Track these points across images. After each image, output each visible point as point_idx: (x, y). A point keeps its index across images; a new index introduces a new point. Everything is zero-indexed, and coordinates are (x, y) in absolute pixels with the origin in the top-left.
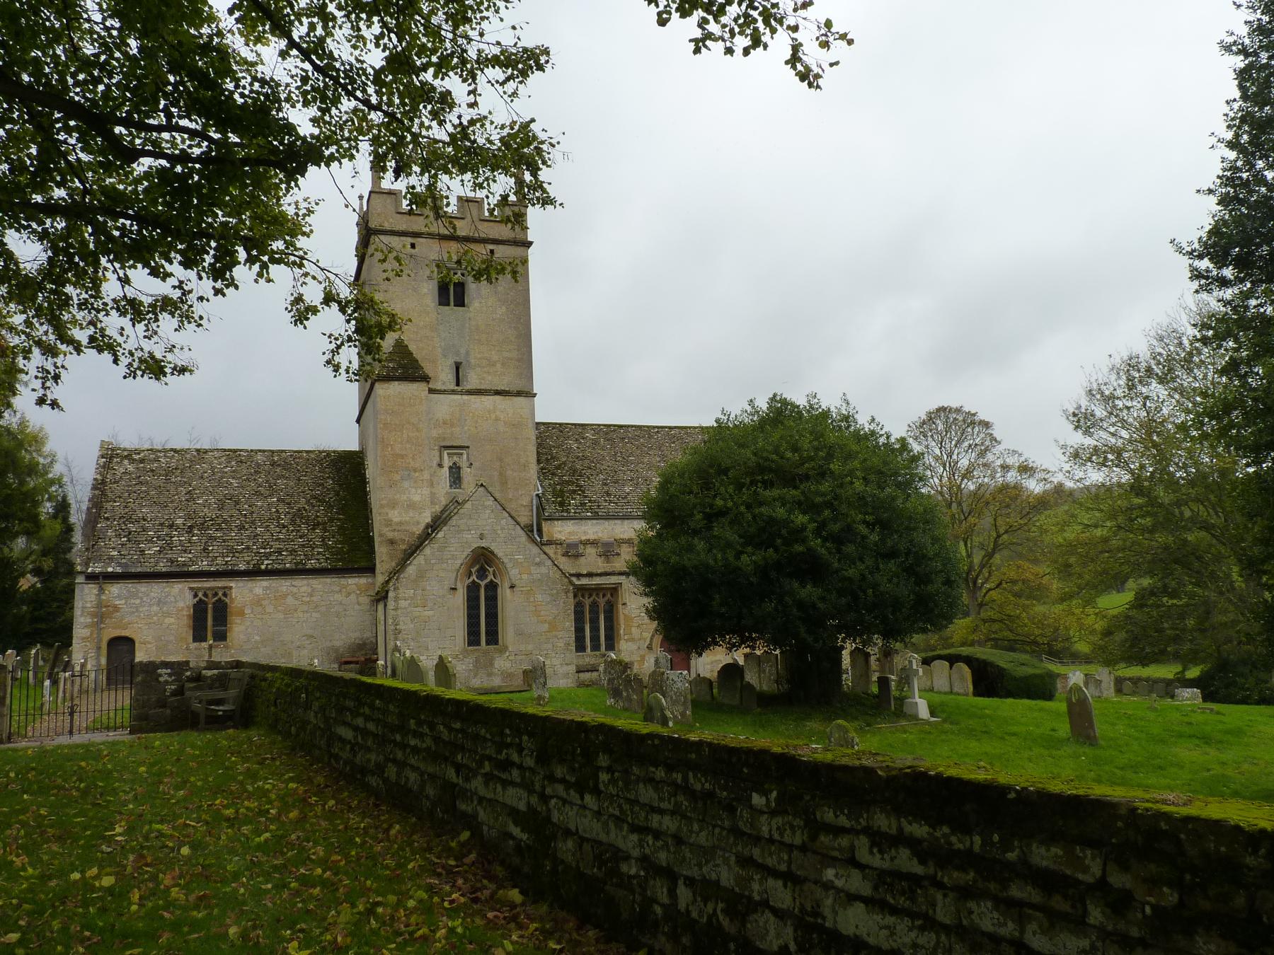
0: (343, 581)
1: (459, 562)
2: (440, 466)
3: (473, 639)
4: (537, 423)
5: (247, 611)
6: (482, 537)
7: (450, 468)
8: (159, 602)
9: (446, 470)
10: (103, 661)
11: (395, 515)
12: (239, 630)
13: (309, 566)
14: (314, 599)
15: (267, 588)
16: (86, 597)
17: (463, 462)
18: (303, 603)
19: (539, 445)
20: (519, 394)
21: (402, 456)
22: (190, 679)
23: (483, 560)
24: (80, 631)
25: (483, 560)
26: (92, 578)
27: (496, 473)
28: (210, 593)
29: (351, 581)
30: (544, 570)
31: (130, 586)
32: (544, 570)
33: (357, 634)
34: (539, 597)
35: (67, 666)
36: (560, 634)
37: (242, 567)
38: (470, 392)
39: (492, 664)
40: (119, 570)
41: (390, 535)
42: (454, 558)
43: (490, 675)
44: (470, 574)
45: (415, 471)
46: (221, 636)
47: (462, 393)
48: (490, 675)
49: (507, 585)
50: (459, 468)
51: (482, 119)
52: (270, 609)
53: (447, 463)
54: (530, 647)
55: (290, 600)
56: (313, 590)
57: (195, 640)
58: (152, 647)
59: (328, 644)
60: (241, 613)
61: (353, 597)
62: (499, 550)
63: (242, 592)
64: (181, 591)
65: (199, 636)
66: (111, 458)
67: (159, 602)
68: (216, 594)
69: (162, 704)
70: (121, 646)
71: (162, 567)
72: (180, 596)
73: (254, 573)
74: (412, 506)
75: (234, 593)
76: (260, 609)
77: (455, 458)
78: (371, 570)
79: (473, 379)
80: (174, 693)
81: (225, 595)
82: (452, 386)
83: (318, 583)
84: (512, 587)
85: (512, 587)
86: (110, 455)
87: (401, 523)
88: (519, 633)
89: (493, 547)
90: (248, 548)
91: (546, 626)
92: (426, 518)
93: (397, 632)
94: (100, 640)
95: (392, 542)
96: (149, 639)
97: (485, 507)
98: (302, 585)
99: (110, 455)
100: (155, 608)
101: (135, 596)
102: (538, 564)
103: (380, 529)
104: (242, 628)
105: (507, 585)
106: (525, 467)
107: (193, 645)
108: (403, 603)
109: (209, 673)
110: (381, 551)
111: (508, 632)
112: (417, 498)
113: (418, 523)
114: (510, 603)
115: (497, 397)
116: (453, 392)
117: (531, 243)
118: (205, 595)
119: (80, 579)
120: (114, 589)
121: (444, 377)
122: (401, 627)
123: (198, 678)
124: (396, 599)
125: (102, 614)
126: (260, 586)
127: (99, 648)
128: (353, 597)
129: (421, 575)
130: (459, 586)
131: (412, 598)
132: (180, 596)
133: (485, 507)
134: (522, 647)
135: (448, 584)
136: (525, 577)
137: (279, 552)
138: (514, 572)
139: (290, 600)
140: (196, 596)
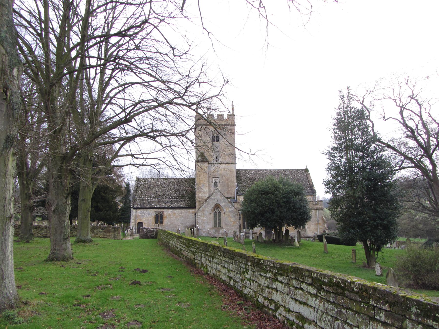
0: (189, 210)
1: (212, 207)
2: (212, 182)
3: (215, 225)
4: (237, 170)
5: (167, 217)
6: (217, 201)
7: (215, 183)
8: (148, 214)
9: (214, 183)
10: (137, 227)
11: (200, 195)
12: (165, 221)
13: (181, 206)
14: (182, 214)
15: (171, 212)
16: (133, 213)
17: (218, 181)
18: (180, 215)
19: (237, 178)
20: (232, 163)
21: (202, 181)
22: (149, 231)
23: (217, 206)
24: (132, 221)
25: (217, 206)
26: (134, 209)
27: (226, 184)
28: (159, 213)
29: (190, 210)
30: (232, 209)
31: (142, 211)
32: (232, 209)
33: (192, 223)
34: (231, 216)
35: (129, 228)
36: (236, 225)
37: (166, 207)
38: (220, 164)
39: (219, 231)
40: (140, 207)
41: (199, 200)
42: (211, 206)
43: (219, 233)
44: (214, 210)
45: (205, 184)
46: (161, 223)
47: (217, 164)
48: (219, 233)
49: (223, 213)
50: (217, 183)
51: (119, 233)
52: (172, 217)
53: (214, 181)
54: (228, 227)
55: (177, 215)
56: (182, 212)
57: (156, 223)
58: (147, 224)
59: (185, 225)
60: (166, 217)
61: (191, 214)
62: (222, 204)
63: (166, 213)
64: (153, 212)
65: (157, 222)
66: (138, 180)
67: (148, 214)
68: (160, 213)
69: (144, 235)
70: (140, 224)
71: (149, 206)
72: (152, 213)
73: (169, 208)
74: (204, 193)
75: (164, 213)
76: (170, 217)
77: (216, 180)
78: (195, 207)
79: (221, 160)
80: (146, 233)
81: (162, 213)
82: (215, 162)
83: (183, 211)
84: (224, 213)
85: (224, 213)
86: (138, 180)
87: (201, 197)
88: (226, 224)
89: (220, 203)
90: (167, 202)
91: (232, 223)
92: (208, 196)
93: (198, 223)
94: (136, 223)
95: (199, 201)
96: (146, 223)
97: (218, 194)
98: (179, 211)
99: (138, 180)
100: (147, 216)
101: (143, 213)
102: (231, 208)
103: (197, 199)
104: (166, 221)
105: (223, 213)
106: (233, 182)
107: (156, 225)
108: (199, 216)
109: (151, 230)
110: (197, 203)
111: (223, 224)
112: (205, 191)
113: (206, 197)
114: (224, 216)
115: (227, 165)
116: (216, 164)
117: (235, 125)
118: (158, 213)
119: (132, 209)
120: (139, 211)
121: (213, 160)
122: (198, 222)
123: (150, 231)
124: (198, 215)
125: (136, 216)
126: (170, 211)
127: (136, 224)
128: (191, 214)
129: (203, 210)
130: (212, 213)
131: (201, 215)
132: (152, 213)
133: (218, 194)
134: (226, 227)
135: (209, 212)
136: (227, 211)
137: (174, 203)
138: (225, 210)
139: (177, 215)
140: (156, 213)
